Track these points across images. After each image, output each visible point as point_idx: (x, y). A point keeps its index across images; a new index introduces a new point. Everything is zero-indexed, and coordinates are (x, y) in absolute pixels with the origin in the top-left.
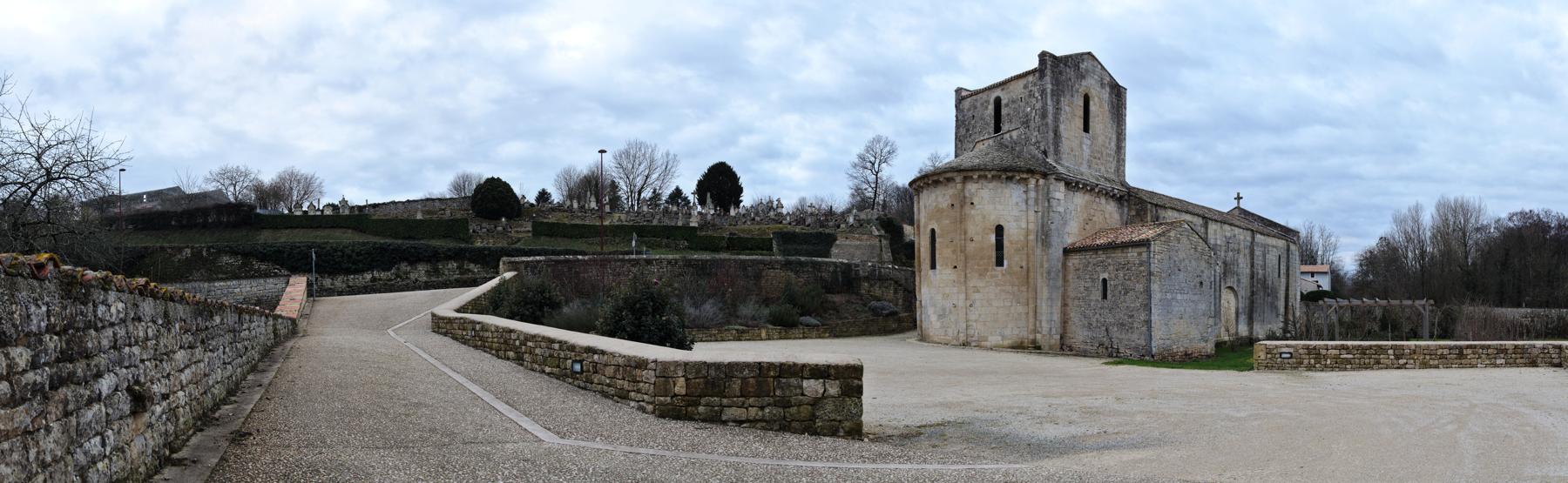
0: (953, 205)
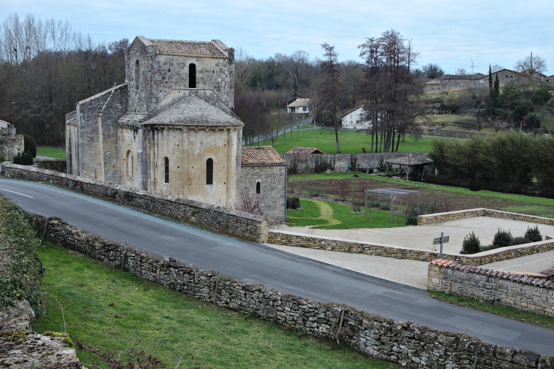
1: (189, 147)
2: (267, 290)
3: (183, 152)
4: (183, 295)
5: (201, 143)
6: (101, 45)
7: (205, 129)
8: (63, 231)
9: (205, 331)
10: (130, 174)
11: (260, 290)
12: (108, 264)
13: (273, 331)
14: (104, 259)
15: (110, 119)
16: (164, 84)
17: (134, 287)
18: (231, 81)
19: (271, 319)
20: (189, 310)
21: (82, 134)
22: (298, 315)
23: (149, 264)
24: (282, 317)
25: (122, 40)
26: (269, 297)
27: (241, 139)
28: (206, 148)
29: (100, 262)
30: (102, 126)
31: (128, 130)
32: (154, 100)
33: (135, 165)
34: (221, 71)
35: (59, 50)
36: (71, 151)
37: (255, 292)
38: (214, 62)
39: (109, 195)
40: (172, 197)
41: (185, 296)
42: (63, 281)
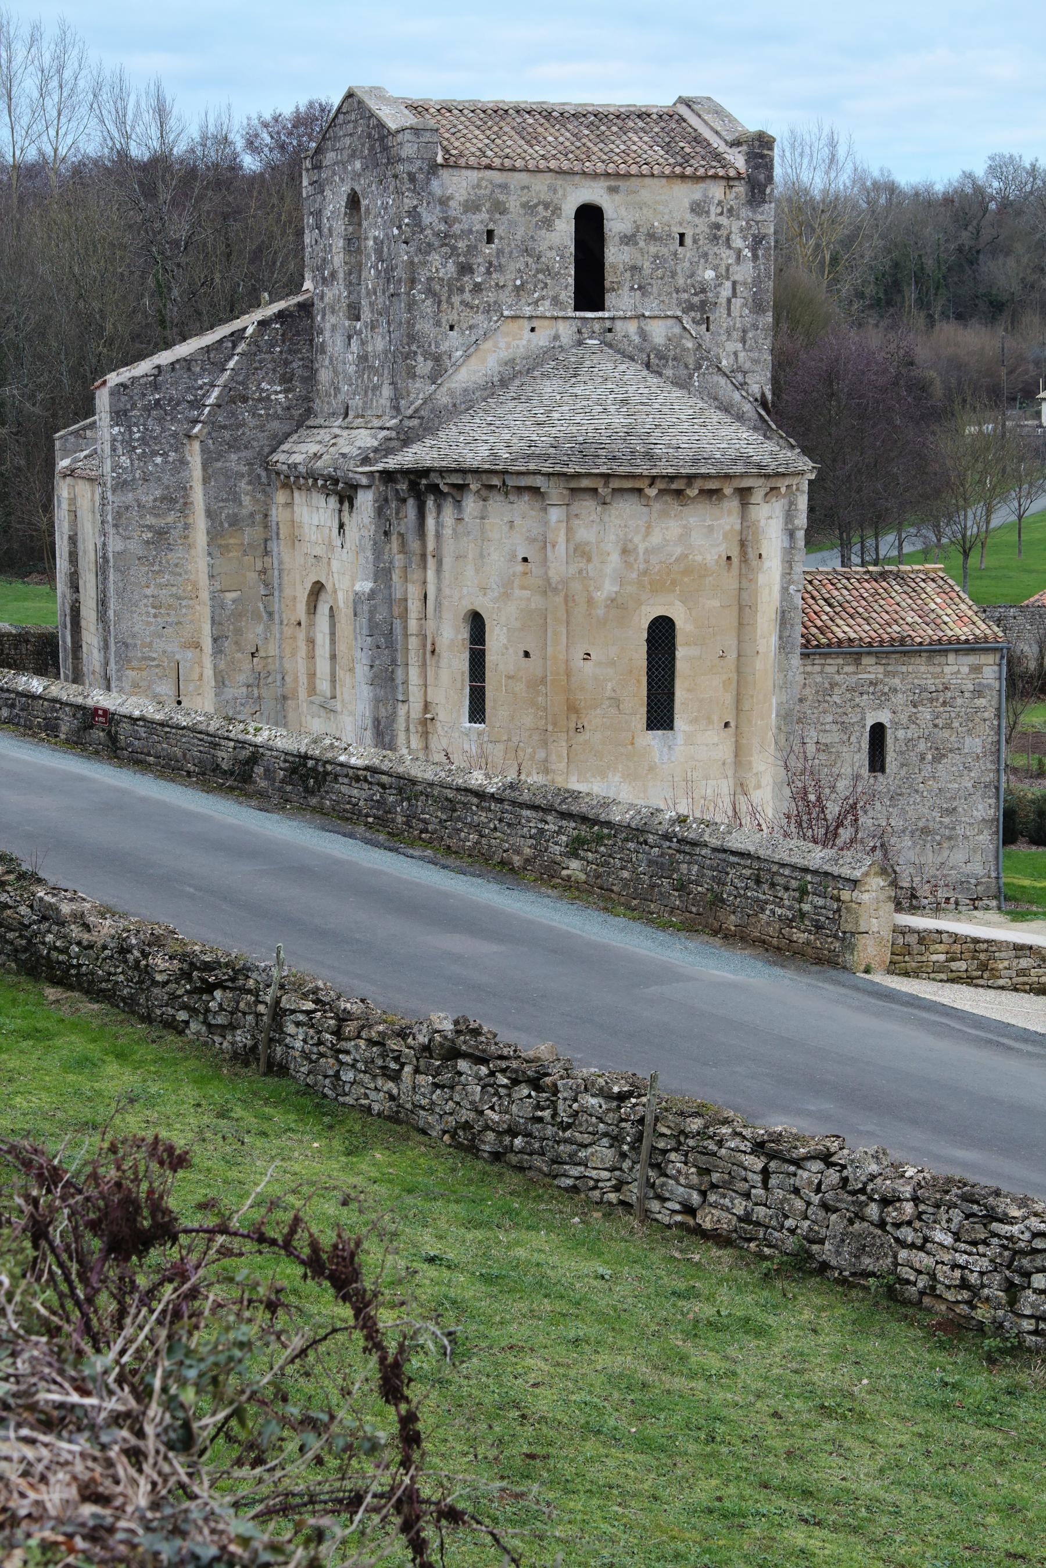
0: (729, 558)
1: (573, 570)
2: (857, 1155)
3: (547, 588)
4: (508, 1173)
5: (625, 551)
6: (212, 129)
7: (640, 491)
8: (23, 910)
9: (588, 1319)
10: (323, 686)
11: (826, 1158)
12: (206, 1043)
13: (877, 1329)
14: (187, 1023)
15: (239, 449)
16: (467, 296)
17: (307, 1137)
18: (757, 281)
19: (871, 1280)
20: (524, 1235)
21: (118, 515)
22: (985, 1264)
23: (371, 1042)
24: (919, 1272)
25: (302, 109)
26: (865, 1184)
27: (801, 534)
28: (645, 572)
29: (170, 1037)
30: (206, 480)
31: (314, 494)
32: (424, 366)
33: (342, 648)
34: (716, 235)
35: (31, 155)
36: (75, 588)
37: (808, 1164)
38: (684, 194)
39: (225, 766)
40: (487, 776)
41: (515, 1180)
42: (13, 1107)
